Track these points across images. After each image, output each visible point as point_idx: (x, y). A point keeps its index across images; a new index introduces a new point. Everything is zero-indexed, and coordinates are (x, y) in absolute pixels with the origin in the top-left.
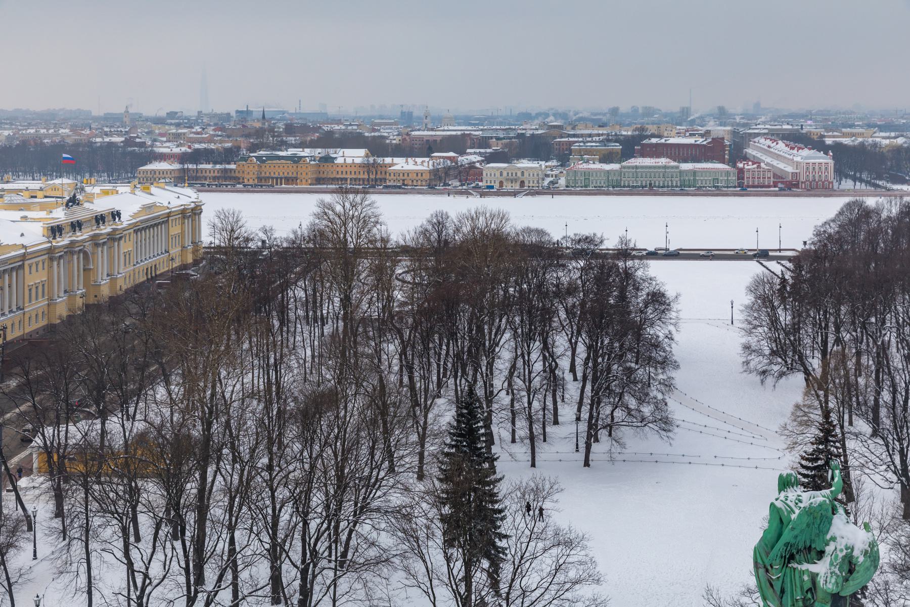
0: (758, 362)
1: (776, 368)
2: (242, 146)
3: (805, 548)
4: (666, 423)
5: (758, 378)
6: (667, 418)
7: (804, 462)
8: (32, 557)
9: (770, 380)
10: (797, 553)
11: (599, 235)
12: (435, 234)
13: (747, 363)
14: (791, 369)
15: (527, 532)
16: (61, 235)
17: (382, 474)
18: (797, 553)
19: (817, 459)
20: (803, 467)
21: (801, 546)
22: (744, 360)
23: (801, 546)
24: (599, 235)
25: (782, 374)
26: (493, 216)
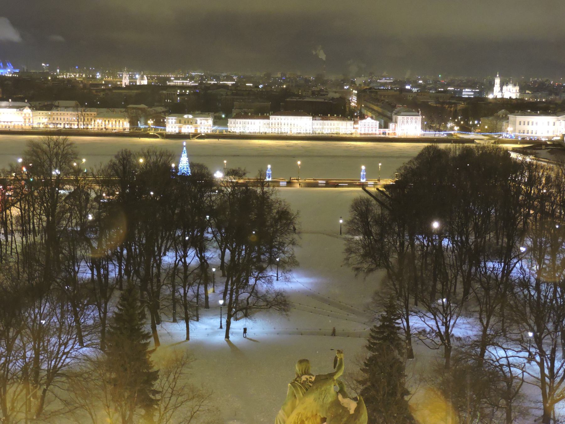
0: (355, 258)
1: (365, 266)
2: (558, 97)
3: (312, 416)
4: (285, 305)
5: (354, 273)
6: (285, 301)
7: (373, 334)
8: (219, 327)
9: (361, 274)
10: (306, 420)
11: (243, 169)
12: (121, 167)
13: (347, 259)
14: (378, 266)
15: (170, 390)
16: (122, 152)
17: (11, 358)
18: (306, 420)
19: (384, 332)
20: (373, 337)
21: (309, 415)
22: (345, 257)
23: (309, 415)
24: (243, 169)
25: (370, 270)
26: (161, 155)
